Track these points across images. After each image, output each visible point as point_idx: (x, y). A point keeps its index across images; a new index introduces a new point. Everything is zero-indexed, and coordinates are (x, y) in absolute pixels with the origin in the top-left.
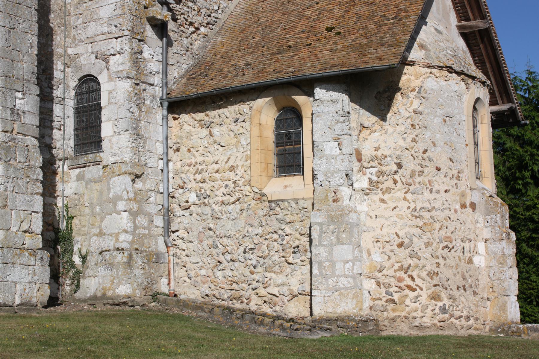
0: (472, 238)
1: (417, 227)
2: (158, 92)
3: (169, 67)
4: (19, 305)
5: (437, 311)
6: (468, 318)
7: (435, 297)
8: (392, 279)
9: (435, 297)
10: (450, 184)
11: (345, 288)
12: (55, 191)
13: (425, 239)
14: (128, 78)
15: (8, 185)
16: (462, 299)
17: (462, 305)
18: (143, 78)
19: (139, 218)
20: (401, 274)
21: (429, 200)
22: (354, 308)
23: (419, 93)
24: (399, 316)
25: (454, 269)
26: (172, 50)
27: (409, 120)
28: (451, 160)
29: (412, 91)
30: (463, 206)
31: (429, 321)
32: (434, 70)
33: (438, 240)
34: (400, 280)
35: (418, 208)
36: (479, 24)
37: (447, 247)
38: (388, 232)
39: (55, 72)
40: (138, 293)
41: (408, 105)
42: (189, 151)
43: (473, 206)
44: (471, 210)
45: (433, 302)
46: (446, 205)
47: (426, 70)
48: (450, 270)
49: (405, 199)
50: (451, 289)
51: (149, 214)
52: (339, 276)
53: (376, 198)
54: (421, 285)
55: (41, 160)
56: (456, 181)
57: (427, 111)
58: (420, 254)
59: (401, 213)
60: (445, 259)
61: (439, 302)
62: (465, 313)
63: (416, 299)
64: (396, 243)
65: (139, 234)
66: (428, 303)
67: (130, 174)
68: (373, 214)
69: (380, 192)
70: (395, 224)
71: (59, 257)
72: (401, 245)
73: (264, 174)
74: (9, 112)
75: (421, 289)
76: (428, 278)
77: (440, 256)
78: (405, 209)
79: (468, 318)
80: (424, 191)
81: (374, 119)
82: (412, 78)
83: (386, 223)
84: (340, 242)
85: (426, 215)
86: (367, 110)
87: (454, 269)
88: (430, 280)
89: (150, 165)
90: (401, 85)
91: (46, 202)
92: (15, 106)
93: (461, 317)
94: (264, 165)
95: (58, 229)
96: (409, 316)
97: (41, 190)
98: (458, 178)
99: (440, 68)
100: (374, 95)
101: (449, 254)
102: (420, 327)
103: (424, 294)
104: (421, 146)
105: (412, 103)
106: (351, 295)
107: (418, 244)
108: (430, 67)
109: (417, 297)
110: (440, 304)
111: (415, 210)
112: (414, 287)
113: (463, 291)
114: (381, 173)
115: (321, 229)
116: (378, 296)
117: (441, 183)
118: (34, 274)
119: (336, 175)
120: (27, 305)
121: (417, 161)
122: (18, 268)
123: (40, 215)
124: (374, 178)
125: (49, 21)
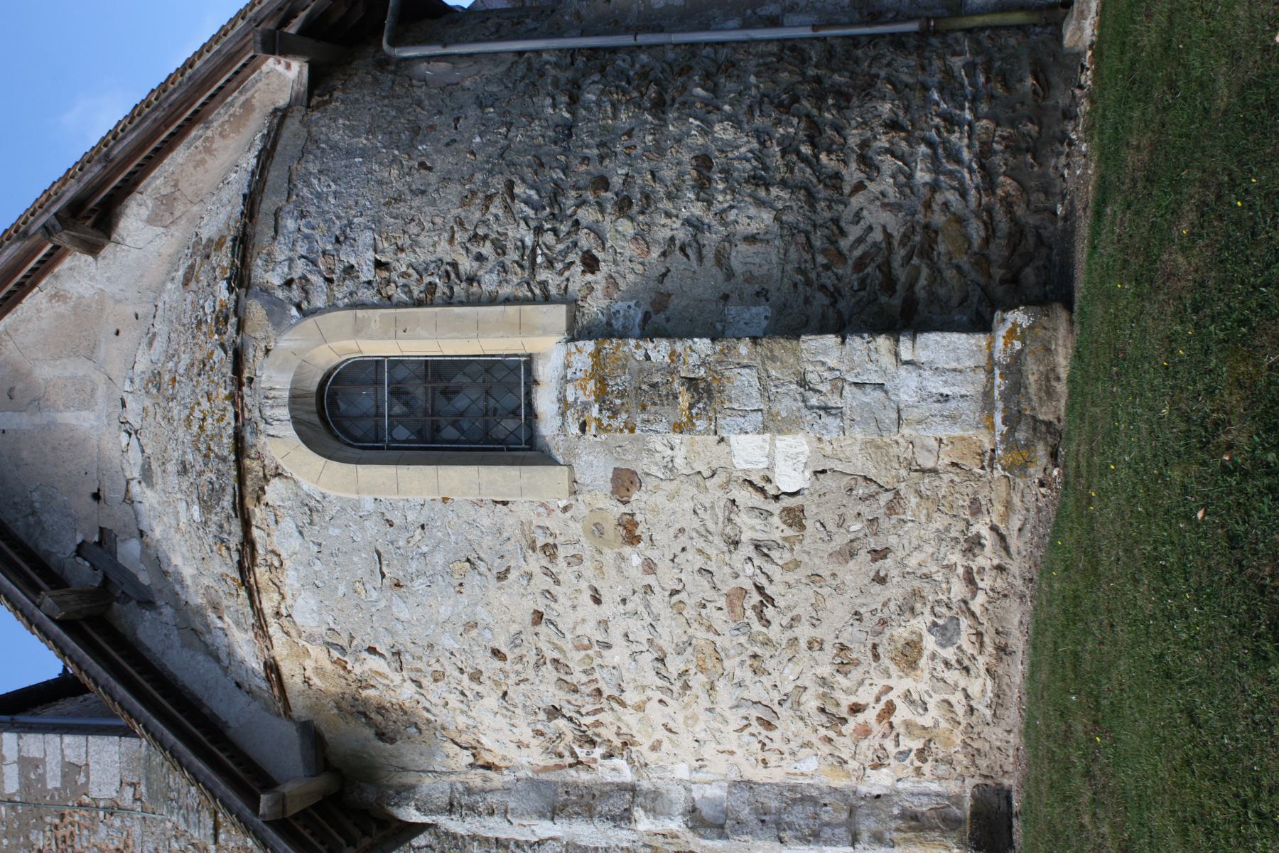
5: (949, 653)
7: (909, 655)
25: (826, 591)
29: (345, 668)
31: (980, 681)
33: (743, 639)
37: (759, 611)
45: (924, 662)
47: (273, 629)
50: (885, 605)
54: (876, 690)
61: (924, 644)
62: (956, 557)
66: (926, 675)
76: (856, 674)
77: (790, 634)
79: (974, 544)
82: (309, 664)
85: (675, 665)
91: (601, 53)
96: (964, 723)
99: (253, 594)
100: (388, 746)
101: (780, 602)
103: (901, 684)
110: (930, 643)
112: (881, 705)
113: (889, 562)
117: (578, 617)
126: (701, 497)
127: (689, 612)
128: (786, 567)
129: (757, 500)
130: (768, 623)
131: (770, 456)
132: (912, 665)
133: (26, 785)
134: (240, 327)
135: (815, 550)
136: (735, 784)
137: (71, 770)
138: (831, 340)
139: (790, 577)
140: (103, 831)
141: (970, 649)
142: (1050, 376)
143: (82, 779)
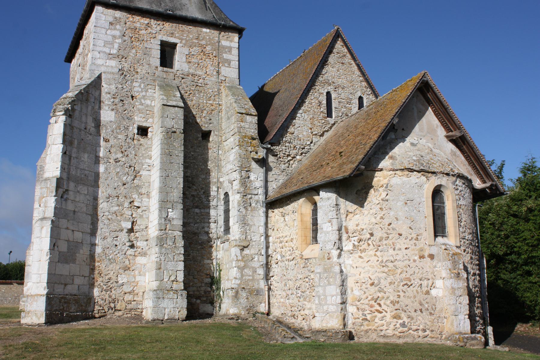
0: (430, 278)
1: (383, 272)
2: (261, 198)
3: (269, 184)
4: (167, 320)
5: (398, 325)
6: (424, 331)
7: (397, 317)
8: (367, 306)
9: (397, 317)
10: (409, 244)
11: (333, 312)
12: (212, 257)
13: (389, 280)
14: (238, 193)
15: (162, 258)
16: (420, 318)
17: (419, 322)
18: (249, 192)
19: (245, 270)
20: (372, 302)
21: (392, 255)
22: (336, 324)
23: (386, 187)
24: (370, 329)
25: (412, 299)
26: (270, 174)
27: (379, 205)
28: (410, 228)
30: (422, 257)
31: (391, 332)
32: (397, 172)
33: (399, 280)
34: (372, 306)
35: (384, 261)
36: (456, 134)
37: (406, 284)
38: (364, 276)
39: (211, 193)
40: (243, 313)
41: (378, 196)
42: (277, 230)
43: (432, 257)
44: (429, 259)
45: (395, 320)
46: (406, 257)
48: (409, 300)
49: (375, 255)
51: (253, 268)
52: (329, 305)
53: (357, 255)
54: (386, 309)
55: (183, 243)
56: (415, 241)
57: (391, 199)
58: (385, 290)
59: (373, 264)
60: (405, 292)
62: (421, 327)
63: (382, 319)
64: (369, 283)
65: (245, 279)
66: (391, 321)
67: (239, 246)
68: (354, 266)
69: (359, 252)
70: (369, 271)
71: (214, 292)
72: (372, 284)
73: (304, 243)
74: (163, 220)
75: (387, 312)
76: (391, 305)
77: (401, 291)
78: (375, 262)
79: (424, 331)
80: (389, 249)
81: (355, 207)
82: (381, 179)
83: (363, 271)
84: (329, 284)
85: (390, 265)
86: (351, 202)
87: (412, 299)
88: (393, 306)
89: (254, 240)
90: (373, 184)
92: (167, 216)
93: (417, 330)
94: (304, 238)
95: (213, 277)
97: (183, 259)
98: (417, 239)
99: (402, 170)
101: (408, 289)
102: (384, 336)
103: (388, 316)
104: (386, 221)
105: (380, 195)
106: (335, 316)
107: (384, 283)
108: (393, 170)
109: (383, 317)
111: (382, 262)
112: (381, 310)
113: (420, 313)
114: (360, 240)
115: (320, 276)
116: (357, 316)
117: (401, 243)
118: (177, 303)
119: (329, 243)
120: (172, 320)
121: (384, 231)
122: (166, 301)
123: (182, 272)
124: (356, 243)
125: (207, 165)
126: (430, 273)
127: (405, 269)
128: (417, 291)
129: (430, 285)
130: (403, 286)
131: (439, 288)
132: (395, 317)
133: (224, 47)
134: (452, 175)
135: (421, 297)
136: (347, 275)
137: (229, 62)
138: (468, 302)
139: (415, 292)
140: (212, 68)
141: (399, 330)
142: (474, 345)
143: (226, 65)
